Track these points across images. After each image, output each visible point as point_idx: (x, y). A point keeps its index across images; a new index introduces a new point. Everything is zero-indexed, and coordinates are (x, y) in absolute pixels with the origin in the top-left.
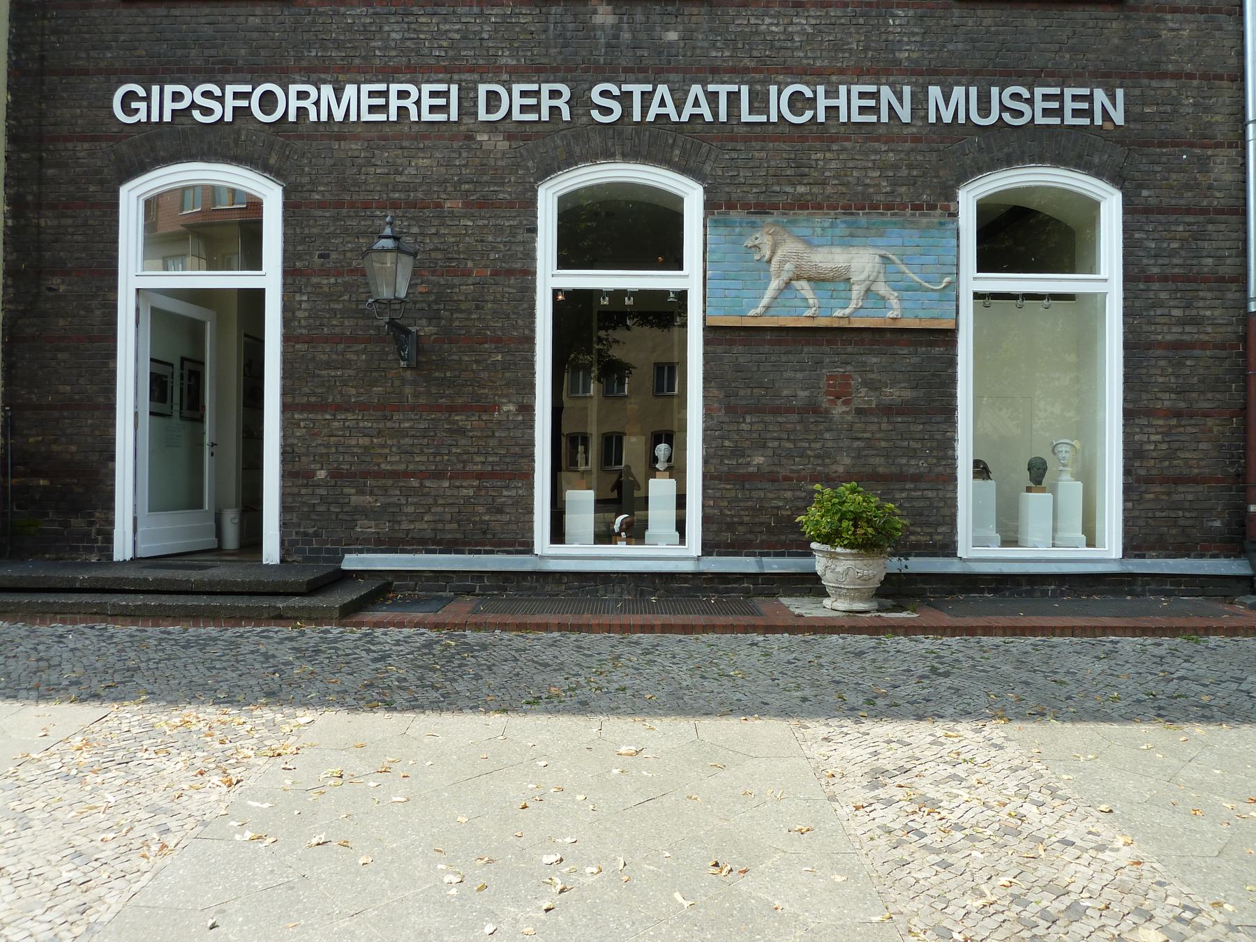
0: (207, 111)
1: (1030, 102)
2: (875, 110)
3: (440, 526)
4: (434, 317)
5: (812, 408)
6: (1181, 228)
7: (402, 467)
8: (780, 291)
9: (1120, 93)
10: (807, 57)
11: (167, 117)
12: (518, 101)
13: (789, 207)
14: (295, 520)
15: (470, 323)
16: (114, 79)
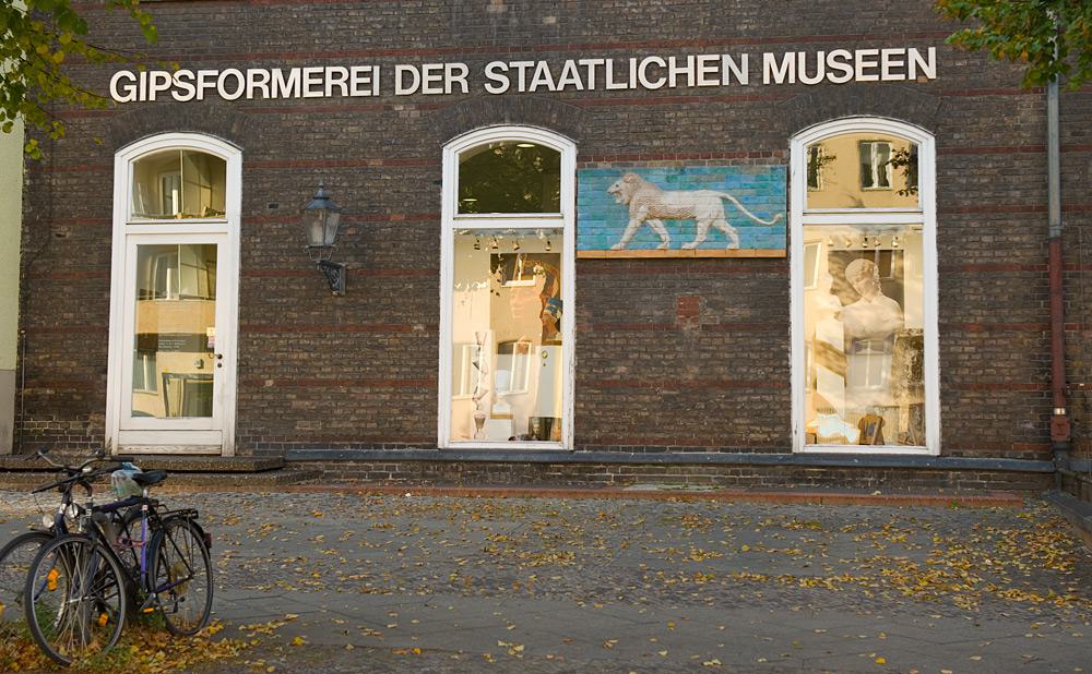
0: (184, 92)
1: (852, 62)
2: (719, 75)
3: (363, 425)
4: (359, 254)
5: (666, 326)
6: (990, 166)
7: (333, 377)
8: (638, 230)
9: (932, 51)
10: (661, 33)
11: (152, 97)
12: (427, 78)
13: (648, 158)
14: (247, 421)
15: (389, 259)
16: (110, 67)
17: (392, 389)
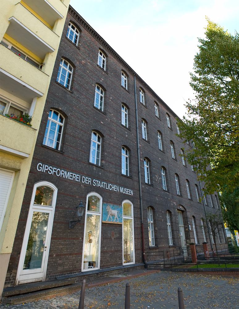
17: (75, 256)
